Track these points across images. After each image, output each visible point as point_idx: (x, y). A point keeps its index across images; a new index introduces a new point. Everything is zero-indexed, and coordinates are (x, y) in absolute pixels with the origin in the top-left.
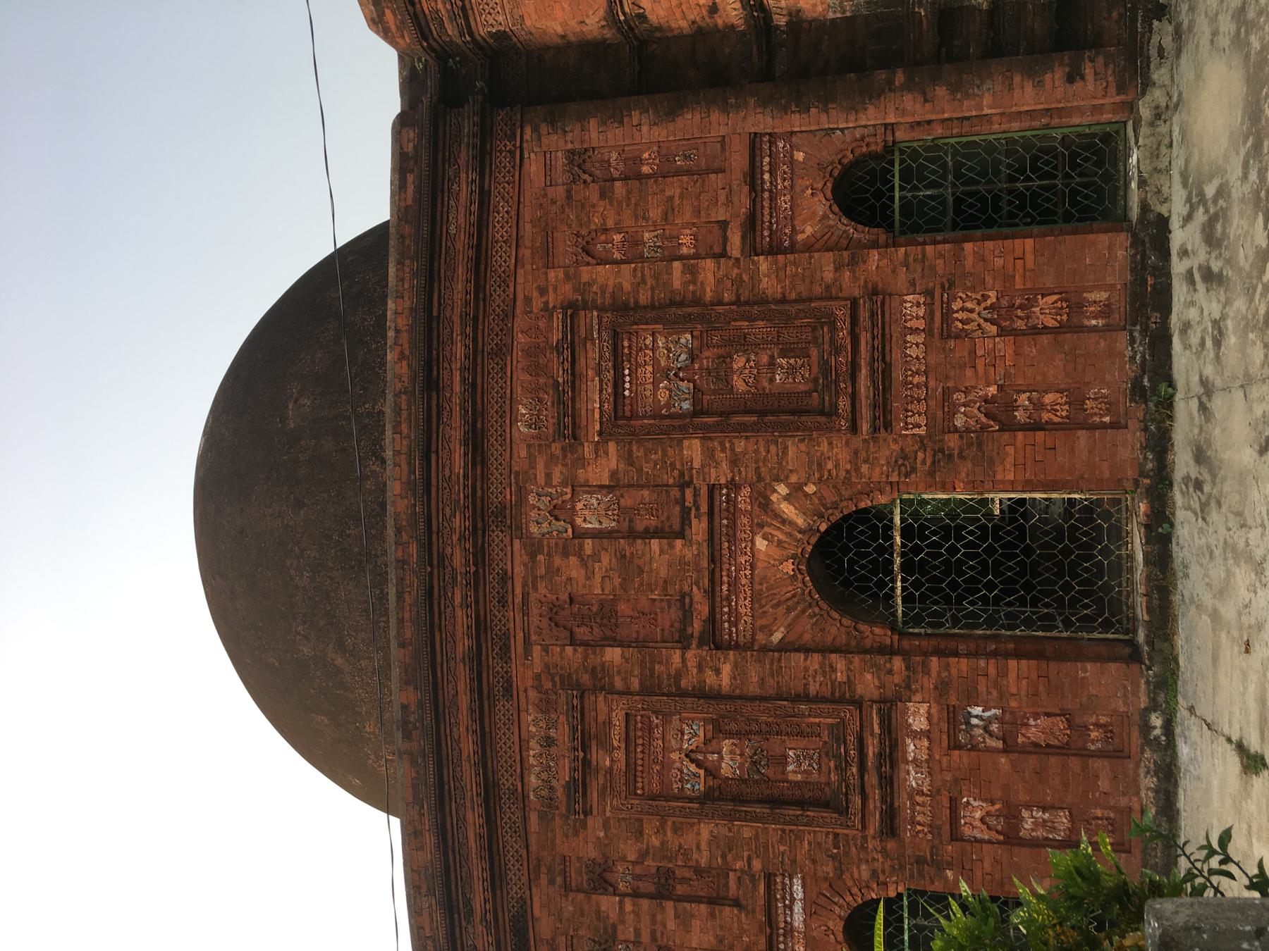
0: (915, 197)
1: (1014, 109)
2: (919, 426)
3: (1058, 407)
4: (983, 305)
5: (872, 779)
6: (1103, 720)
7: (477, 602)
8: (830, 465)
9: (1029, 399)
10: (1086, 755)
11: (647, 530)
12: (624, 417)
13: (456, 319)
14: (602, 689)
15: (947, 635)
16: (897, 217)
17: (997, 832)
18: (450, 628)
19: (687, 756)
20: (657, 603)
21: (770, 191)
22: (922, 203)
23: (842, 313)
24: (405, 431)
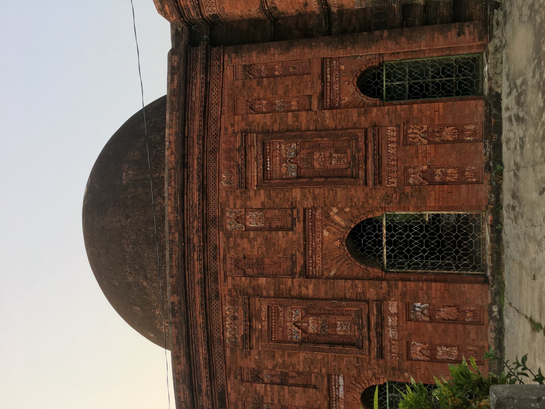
0: (392, 85)
1: (435, 47)
2: (394, 183)
4: (421, 131)
5: (373, 334)
6: (472, 308)
7: (204, 258)
8: (355, 200)
9: (441, 171)
10: (464, 323)
11: (277, 227)
12: (267, 179)
14: (258, 295)
17: (427, 356)
18: (192, 269)
19: (294, 324)
21: (330, 83)
24: (173, 185)
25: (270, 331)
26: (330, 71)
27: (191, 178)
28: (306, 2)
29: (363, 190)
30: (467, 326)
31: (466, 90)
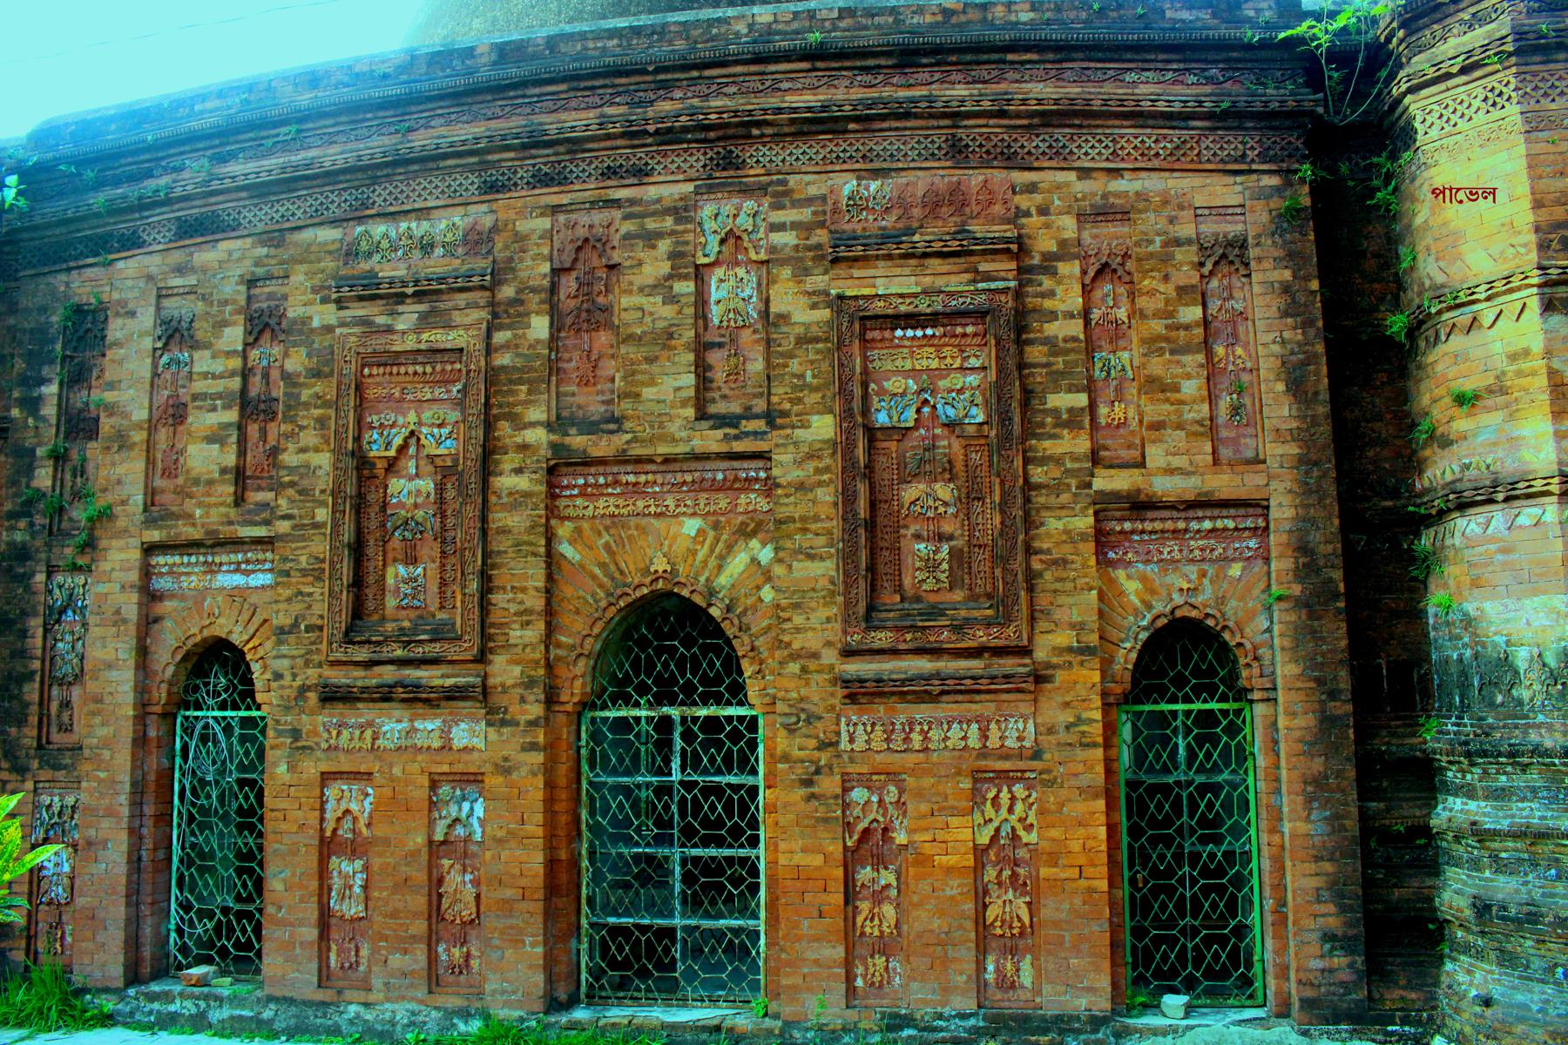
0: (1175, 731)
1: (1288, 864)
2: (852, 741)
3: (876, 922)
4: (1018, 826)
5: (388, 674)
6: (475, 963)
7: (609, 137)
8: (798, 620)
9: (888, 886)
10: (431, 941)
11: (709, 368)
12: (864, 330)
13: (1003, 86)
14: (495, 315)
15: (579, 774)
16: (1147, 708)
17: (335, 830)
18: (573, 104)
19: (412, 433)
20: (609, 385)
21: (1186, 530)
22: (1165, 741)
23: (1010, 635)
24: (842, 24)
25: (392, 359)
26: (1225, 529)
27: (868, 78)
28: (1451, 443)
29: (829, 644)
30: (424, 946)
31: (1148, 957)
